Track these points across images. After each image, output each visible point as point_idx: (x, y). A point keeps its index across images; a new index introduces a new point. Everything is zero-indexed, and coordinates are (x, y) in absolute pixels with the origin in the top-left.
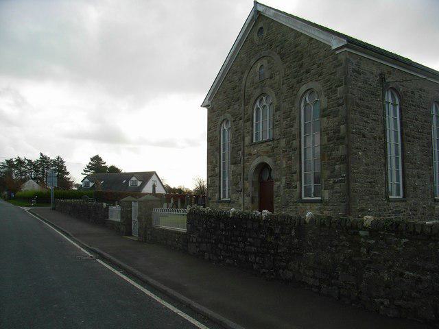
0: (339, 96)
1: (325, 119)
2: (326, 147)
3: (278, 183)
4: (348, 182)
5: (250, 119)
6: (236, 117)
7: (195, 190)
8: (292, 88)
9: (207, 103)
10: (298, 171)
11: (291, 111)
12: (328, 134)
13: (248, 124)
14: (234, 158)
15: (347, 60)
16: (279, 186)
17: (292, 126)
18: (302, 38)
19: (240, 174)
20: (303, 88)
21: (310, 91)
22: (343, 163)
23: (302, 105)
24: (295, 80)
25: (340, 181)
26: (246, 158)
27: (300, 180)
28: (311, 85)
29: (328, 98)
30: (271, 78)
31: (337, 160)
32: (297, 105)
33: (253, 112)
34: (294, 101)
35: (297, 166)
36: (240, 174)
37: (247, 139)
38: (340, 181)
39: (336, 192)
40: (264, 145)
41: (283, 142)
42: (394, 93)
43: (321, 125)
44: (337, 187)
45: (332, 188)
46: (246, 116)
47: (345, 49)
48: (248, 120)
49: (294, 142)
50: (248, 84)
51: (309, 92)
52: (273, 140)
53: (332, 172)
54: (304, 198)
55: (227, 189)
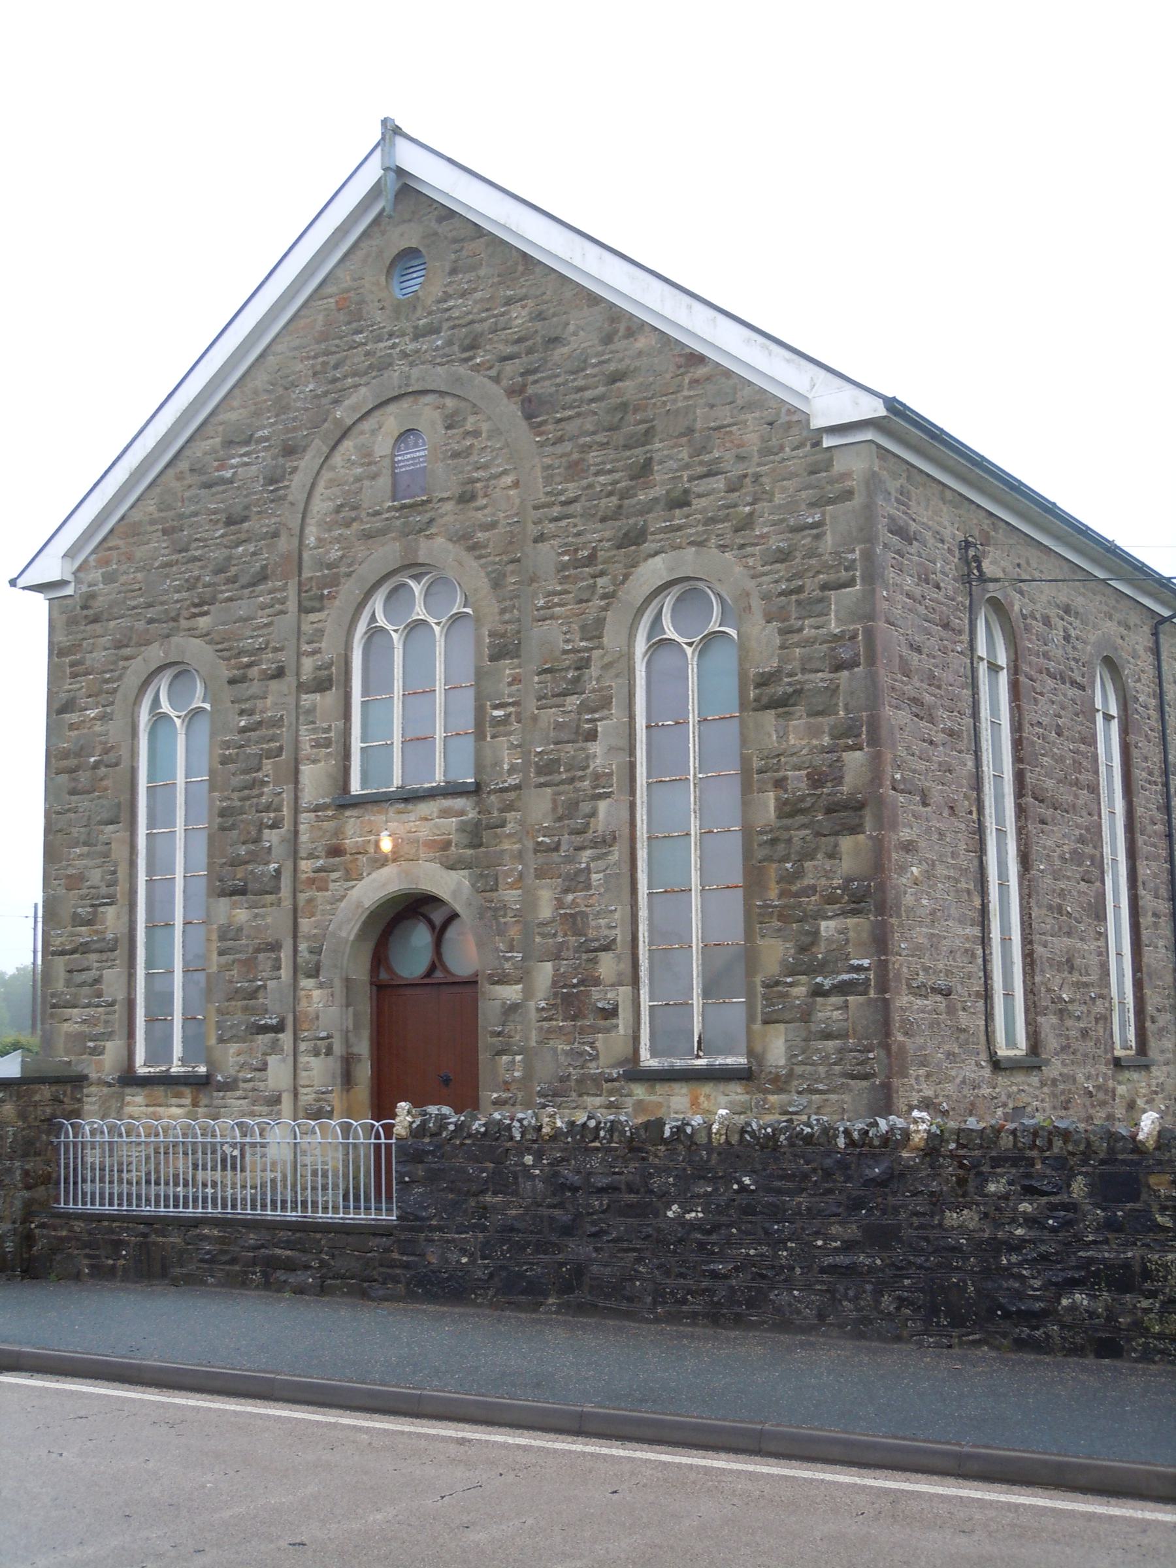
0: (834, 627)
1: (769, 717)
2: (774, 842)
3: (512, 993)
4: (883, 987)
5: (335, 679)
6: (241, 674)
7: (13, 977)
8: (591, 559)
9: (52, 568)
10: (621, 935)
11: (583, 665)
12: (780, 784)
13: (325, 701)
14: (236, 862)
15: (873, 482)
16: (512, 1009)
17: (592, 736)
18: (641, 343)
19: (275, 947)
20: (654, 570)
21: (688, 591)
22: (855, 912)
23: (641, 645)
24: (609, 531)
25: (843, 989)
26: (305, 865)
27: (635, 982)
28: (688, 561)
29: (783, 632)
30: (466, 499)
31: (831, 900)
32: (612, 639)
33: (348, 647)
34: (600, 622)
35: (620, 914)
36: (275, 947)
37: (314, 779)
38: (843, 989)
39: (828, 1036)
40: (424, 808)
41: (539, 806)
42: (994, 619)
43: (744, 742)
44: (829, 1012)
45: (806, 1016)
46: (308, 664)
47: (869, 435)
48: (321, 685)
49: (603, 806)
50: (321, 506)
51: (676, 591)
52: (476, 791)
53: (803, 949)
54: (647, 1060)
55: (62, 1161)
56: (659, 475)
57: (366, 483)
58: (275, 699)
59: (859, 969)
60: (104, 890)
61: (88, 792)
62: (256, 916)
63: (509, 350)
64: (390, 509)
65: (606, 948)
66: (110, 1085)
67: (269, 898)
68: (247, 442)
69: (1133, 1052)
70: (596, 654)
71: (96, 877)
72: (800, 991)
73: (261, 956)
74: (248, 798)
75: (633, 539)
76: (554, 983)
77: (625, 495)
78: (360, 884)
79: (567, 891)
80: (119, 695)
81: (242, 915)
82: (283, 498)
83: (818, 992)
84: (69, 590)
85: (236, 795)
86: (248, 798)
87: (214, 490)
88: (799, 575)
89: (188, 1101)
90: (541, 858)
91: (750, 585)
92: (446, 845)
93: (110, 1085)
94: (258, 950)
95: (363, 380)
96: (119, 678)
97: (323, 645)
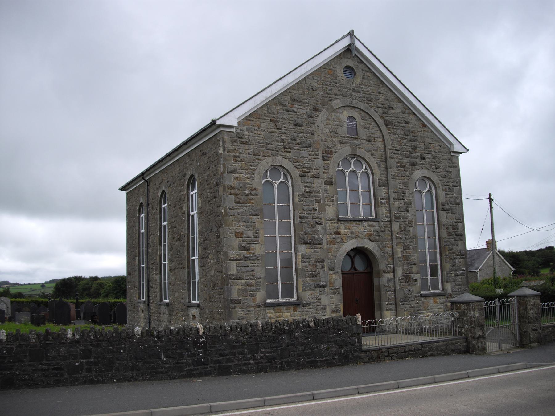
44: (458, 279)
56: (418, 150)
57: (340, 127)
58: (317, 184)
59: (463, 270)
60: (253, 239)
61: (245, 203)
62: (315, 251)
63: (380, 105)
64: (347, 137)
65: (415, 264)
66: (259, 306)
67: (319, 246)
68: (300, 102)
69: (342, 313)
70: (407, 191)
71: (250, 233)
72: (453, 275)
73: (318, 264)
74: (310, 214)
75: (413, 164)
76: (403, 273)
77: (410, 152)
78: (346, 244)
79: (404, 249)
80: (256, 171)
81: (309, 251)
82: (314, 123)
83: (457, 275)
84: (233, 130)
85: (305, 212)
86: (310, 214)
87: (290, 113)
88: (448, 182)
89: (292, 310)
90: (398, 241)
91: (439, 182)
92: (371, 235)
93: (259, 306)
94: (316, 262)
95: (338, 97)
96: (256, 166)
97: (329, 171)
